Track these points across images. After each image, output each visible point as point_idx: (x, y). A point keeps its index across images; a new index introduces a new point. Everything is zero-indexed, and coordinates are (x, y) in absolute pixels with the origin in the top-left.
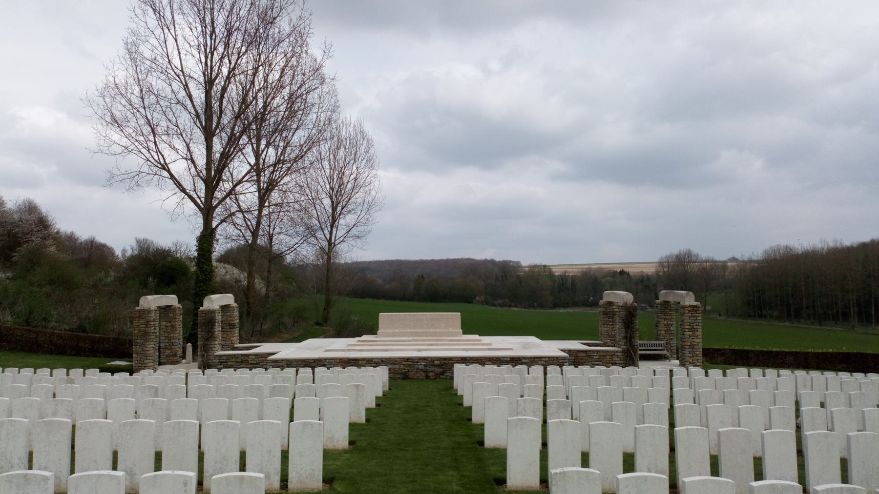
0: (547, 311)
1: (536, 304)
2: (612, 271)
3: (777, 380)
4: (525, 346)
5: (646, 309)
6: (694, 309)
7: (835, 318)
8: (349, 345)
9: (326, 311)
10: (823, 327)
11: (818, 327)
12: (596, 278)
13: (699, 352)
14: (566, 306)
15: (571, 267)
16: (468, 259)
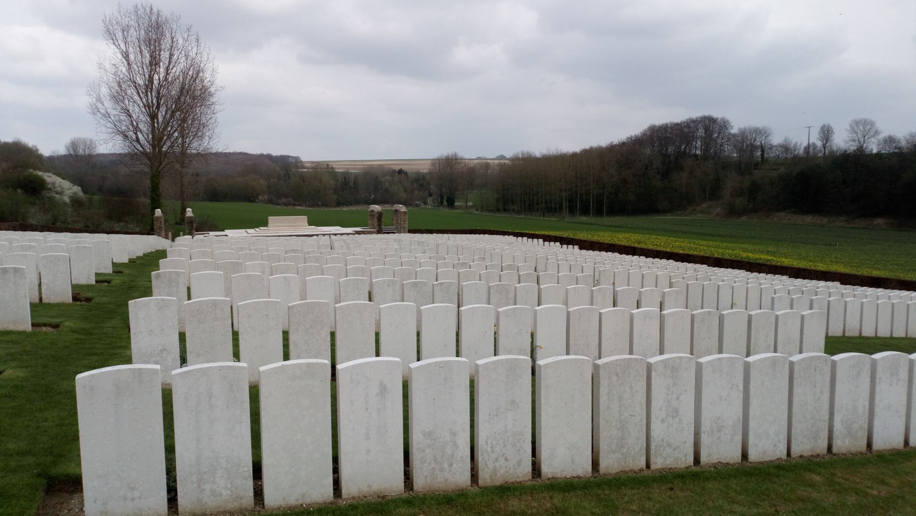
0: (331, 209)
1: (320, 203)
2: (391, 171)
4: (336, 230)
5: (420, 205)
6: (405, 213)
9: (183, 214)
11: (542, 218)
12: (377, 177)
15: (353, 163)
16: (241, 153)
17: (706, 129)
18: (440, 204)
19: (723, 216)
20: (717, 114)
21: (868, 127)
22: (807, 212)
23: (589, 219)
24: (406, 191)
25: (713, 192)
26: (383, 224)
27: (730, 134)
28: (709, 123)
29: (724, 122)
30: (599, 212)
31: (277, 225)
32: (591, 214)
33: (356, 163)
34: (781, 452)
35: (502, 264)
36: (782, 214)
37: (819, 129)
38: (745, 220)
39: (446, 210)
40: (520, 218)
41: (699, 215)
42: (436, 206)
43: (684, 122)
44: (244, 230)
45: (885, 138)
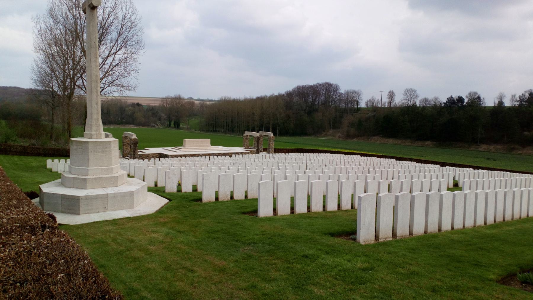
8: (180, 150)
13: (273, 150)
16: (15, 88)
17: (327, 90)
18: (169, 126)
20: (333, 82)
21: (413, 93)
25: (335, 124)
27: (340, 93)
29: (336, 86)
31: (191, 145)
35: (412, 179)
36: (376, 138)
37: (388, 93)
38: (356, 140)
39: (175, 131)
40: (228, 136)
41: (329, 137)
43: (315, 85)
44: (162, 148)
45: (423, 99)
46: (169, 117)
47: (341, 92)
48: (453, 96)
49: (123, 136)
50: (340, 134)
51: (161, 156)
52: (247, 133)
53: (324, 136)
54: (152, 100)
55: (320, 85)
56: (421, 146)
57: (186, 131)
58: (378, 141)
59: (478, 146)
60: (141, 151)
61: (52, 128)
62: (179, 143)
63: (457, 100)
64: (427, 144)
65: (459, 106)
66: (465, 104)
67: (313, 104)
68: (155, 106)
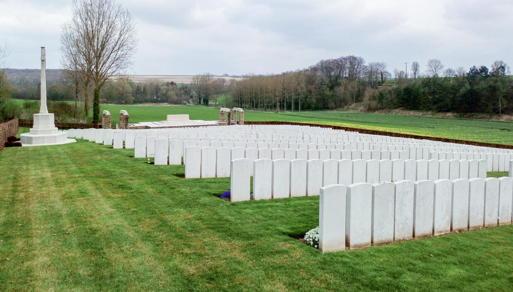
1: (123, 102)
3: (251, 130)
5: (186, 104)
7: (271, 108)
10: (267, 112)
11: (264, 112)
12: (157, 86)
14: (141, 102)
17: (351, 63)
18: (199, 103)
19: (365, 112)
20: (357, 55)
21: (437, 64)
22: (411, 109)
23: (291, 112)
24: (177, 95)
25: (358, 98)
26: (231, 119)
27: (364, 66)
28: (353, 60)
30: (297, 109)
32: (292, 110)
33: (138, 77)
34: (392, 238)
36: (397, 110)
37: (412, 65)
39: (204, 108)
41: (351, 111)
42: (196, 104)
43: (339, 59)
44: (151, 122)
45: (447, 69)
46: (199, 95)
47: (365, 65)
48: (476, 66)
49: (120, 113)
50: (362, 107)
51: (147, 127)
52: (222, 109)
53: (346, 110)
54: (188, 78)
55: (344, 59)
56: (441, 118)
57: (213, 108)
58: (399, 113)
59: (500, 116)
60: (133, 125)
61: (76, 108)
62: (165, 118)
63: (480, 70)
64: (447, 115)
65: (482, 76)
66: (489, 73)
67: (338, 77)
68: (188, 84)
